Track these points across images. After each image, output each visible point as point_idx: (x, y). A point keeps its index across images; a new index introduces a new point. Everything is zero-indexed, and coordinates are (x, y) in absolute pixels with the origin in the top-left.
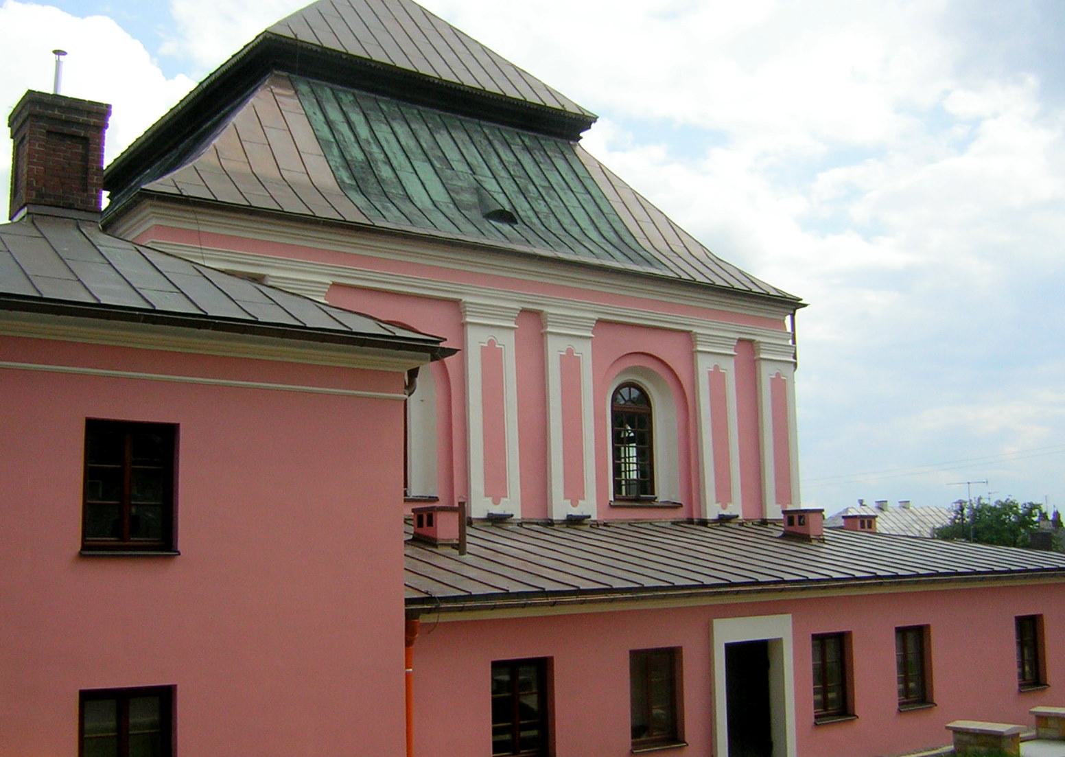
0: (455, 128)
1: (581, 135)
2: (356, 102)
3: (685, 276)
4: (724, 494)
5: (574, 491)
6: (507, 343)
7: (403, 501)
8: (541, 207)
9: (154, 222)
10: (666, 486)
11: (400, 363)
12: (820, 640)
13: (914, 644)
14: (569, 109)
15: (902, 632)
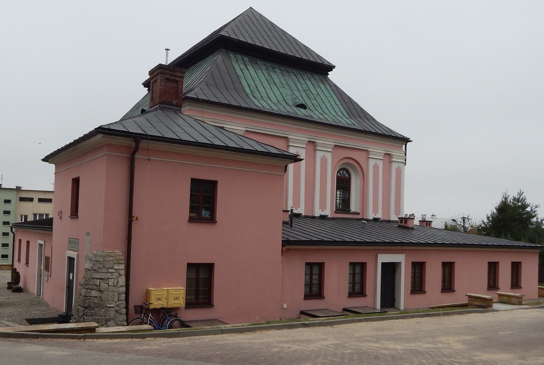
0: (276, 68)
2: (250, 61)
3: (367, 130)
4: (375, 211)
6: (380, 164)
7: (36, 212)
8: (314, 102)
9: (188, 108)
10: (354, 207)
11: (282, 163)
12: (414, 264)
13: (448, 268)
14: (325, 63)
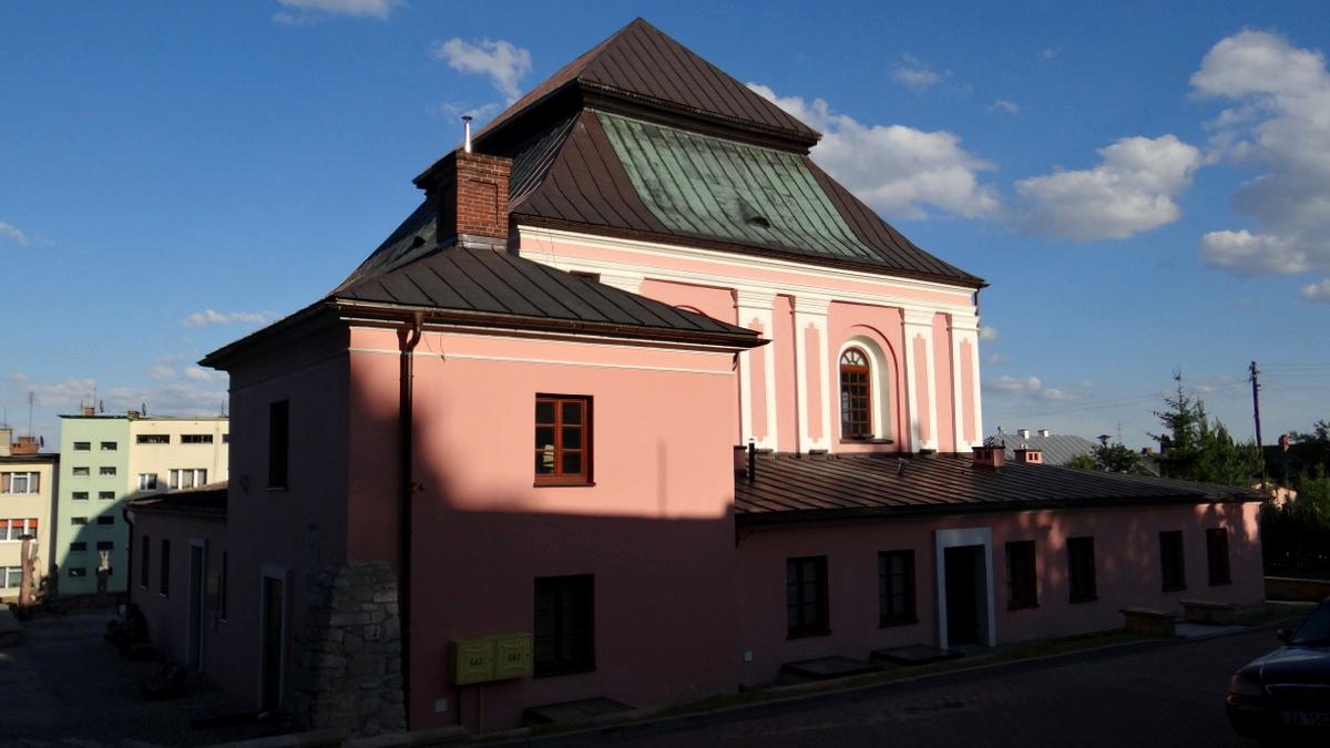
1: (810, 149)
5: (816, 432)
8: (785, 212)
15: (796, 564)
